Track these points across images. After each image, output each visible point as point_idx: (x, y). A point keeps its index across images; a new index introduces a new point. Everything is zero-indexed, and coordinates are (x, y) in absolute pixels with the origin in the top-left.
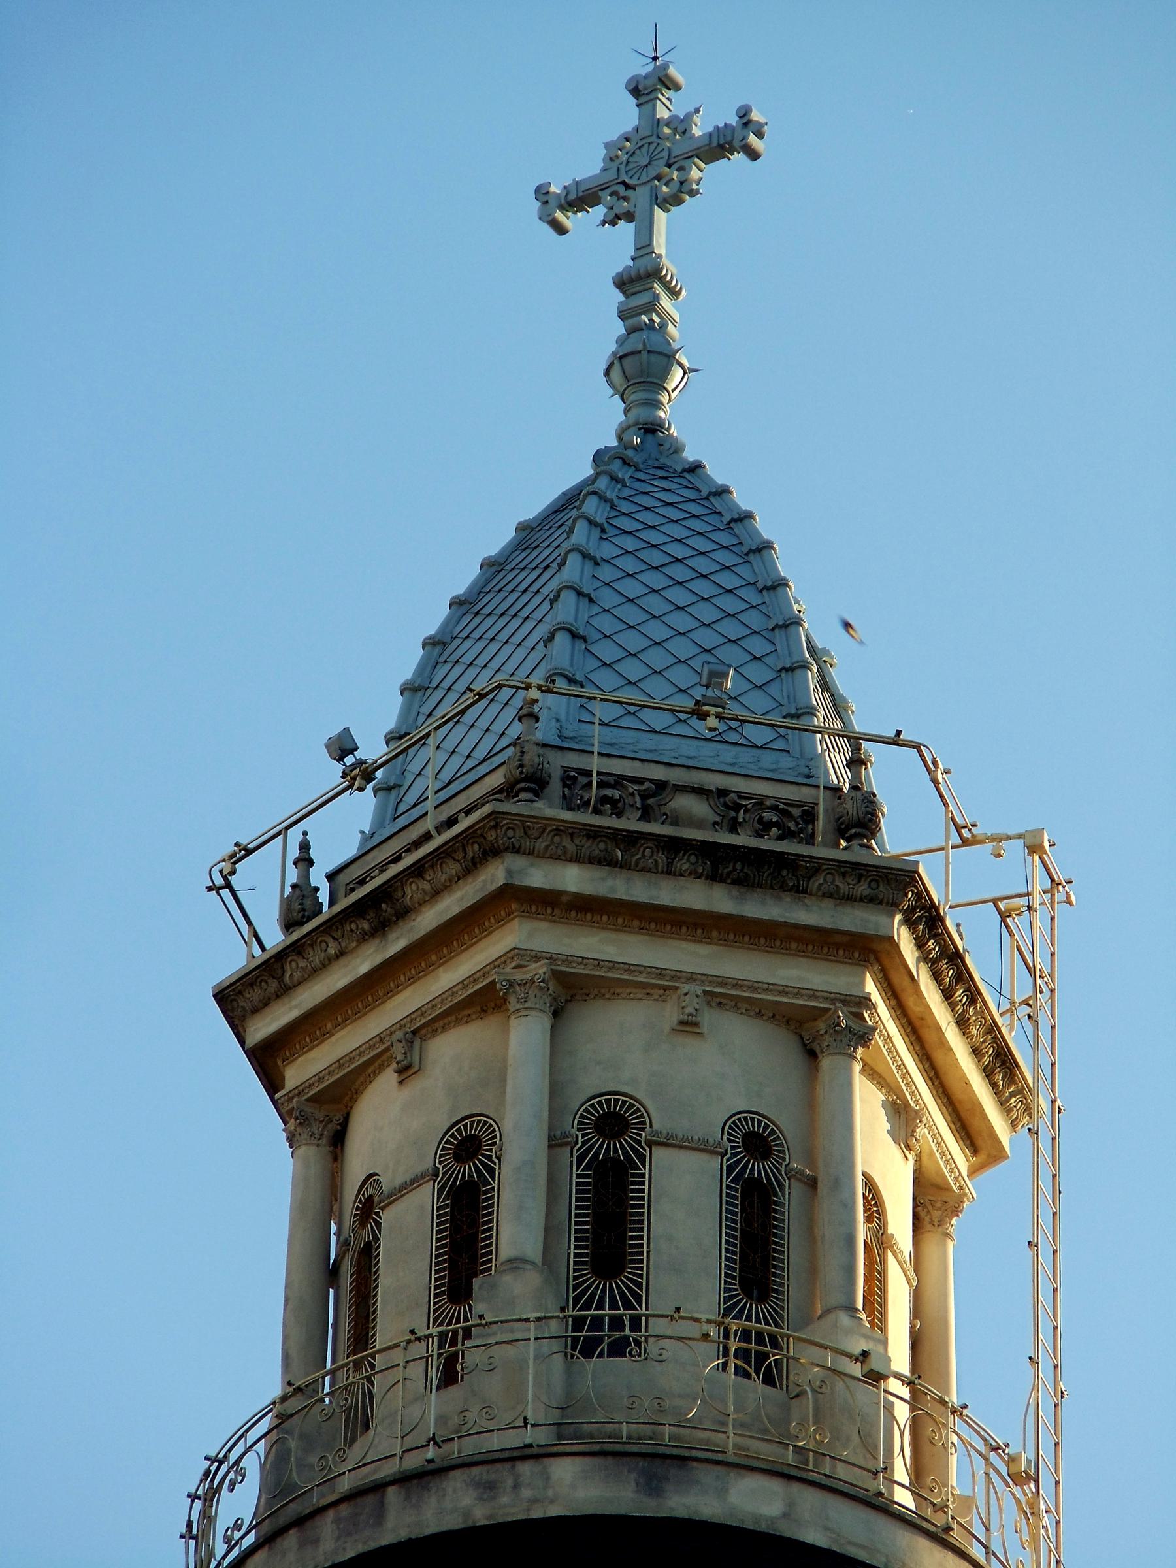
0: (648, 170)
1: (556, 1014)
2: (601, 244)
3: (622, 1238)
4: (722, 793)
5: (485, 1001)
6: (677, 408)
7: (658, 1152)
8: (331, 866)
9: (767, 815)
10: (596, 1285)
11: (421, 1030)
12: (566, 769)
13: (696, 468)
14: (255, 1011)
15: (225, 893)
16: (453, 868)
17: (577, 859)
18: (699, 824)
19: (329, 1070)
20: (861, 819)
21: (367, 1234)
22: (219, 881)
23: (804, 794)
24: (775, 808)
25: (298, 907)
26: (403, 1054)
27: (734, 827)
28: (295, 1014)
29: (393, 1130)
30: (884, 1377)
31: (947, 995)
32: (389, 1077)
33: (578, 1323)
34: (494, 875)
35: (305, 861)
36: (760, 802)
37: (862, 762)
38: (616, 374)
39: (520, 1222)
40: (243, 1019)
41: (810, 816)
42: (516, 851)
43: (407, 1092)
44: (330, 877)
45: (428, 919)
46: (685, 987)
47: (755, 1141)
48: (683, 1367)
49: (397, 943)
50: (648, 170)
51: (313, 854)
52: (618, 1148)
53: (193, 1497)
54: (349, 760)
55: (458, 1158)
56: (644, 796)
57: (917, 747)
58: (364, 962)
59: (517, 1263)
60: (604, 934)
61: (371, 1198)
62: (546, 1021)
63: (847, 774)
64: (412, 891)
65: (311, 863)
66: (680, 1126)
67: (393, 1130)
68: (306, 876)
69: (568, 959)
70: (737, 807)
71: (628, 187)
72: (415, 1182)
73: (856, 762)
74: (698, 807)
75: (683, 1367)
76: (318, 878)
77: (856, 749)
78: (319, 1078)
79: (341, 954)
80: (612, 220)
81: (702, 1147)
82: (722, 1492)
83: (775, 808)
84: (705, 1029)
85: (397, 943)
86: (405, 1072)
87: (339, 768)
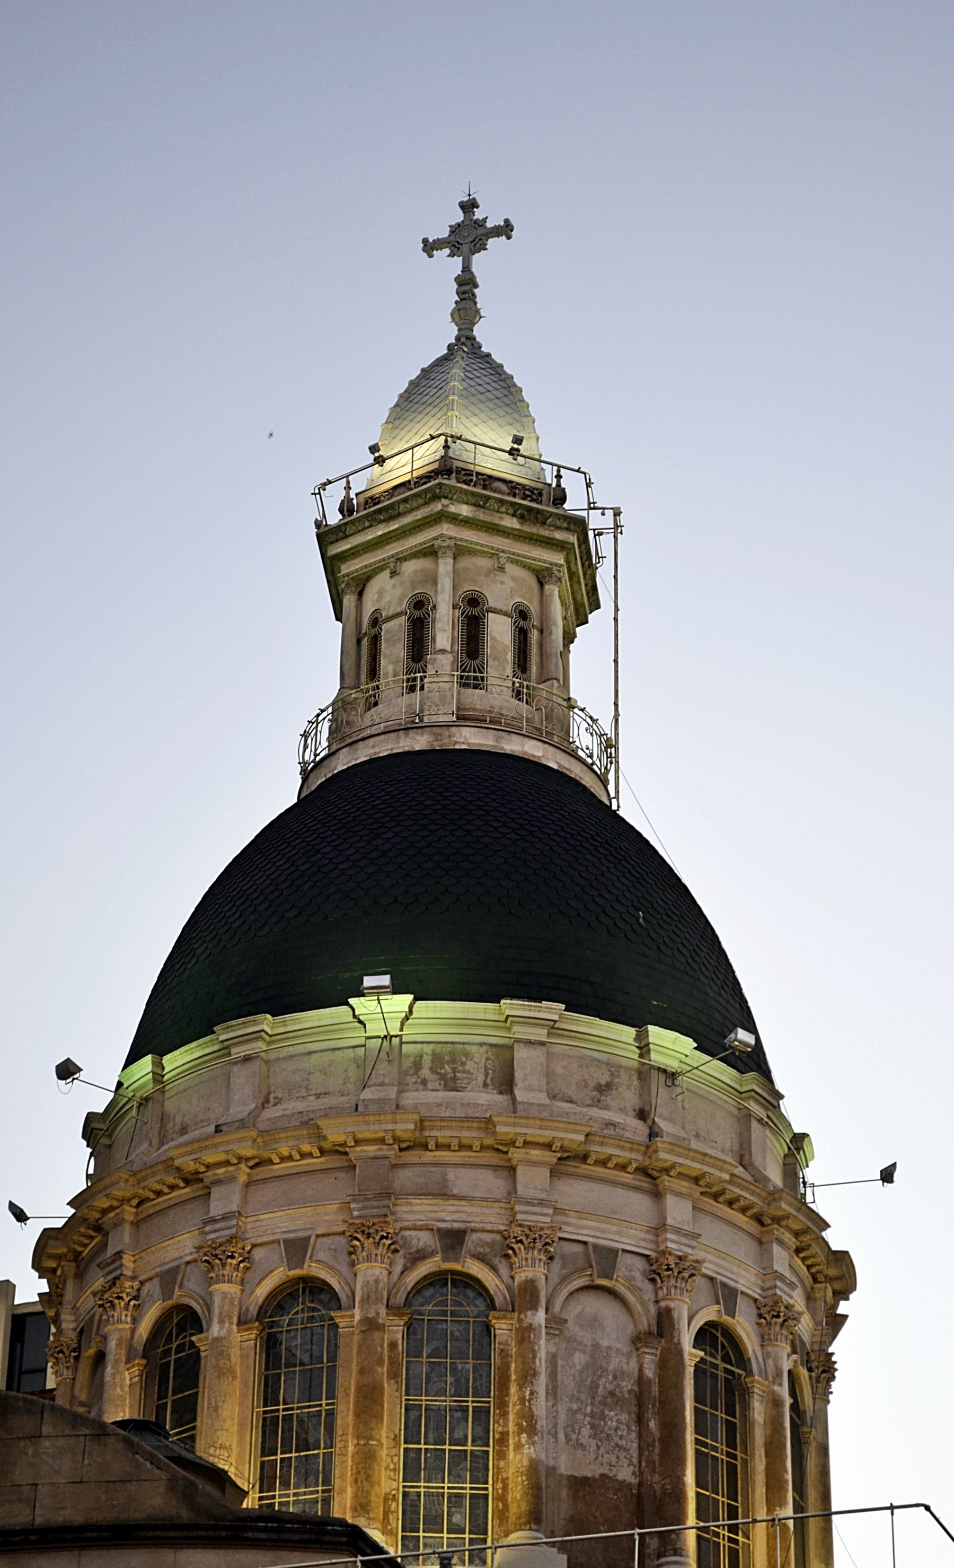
0: (469, 235)
1: (454, 558)
2: (449, 266)
3: (478, 644)
4: (511, 482)
5: (430, 552)
6: (479, 332)
7: (490, 614)
8: (358, 491)
9: (527, 492)
10: (468, 662)
11: (401, 559)
12: (457, 467)
13: (488, 355)
14: (332, 543)
15: (318, 496)
16: (421, 501)
17: (467, 503)
18: (503, 493)
19: (361, 569)
20: (560, 497)
21: (375, 631)
22: (317, 491)
23: (540, 486)
24: (529, 490)
25: (346, 508)
26: (393, 566)
27: (514, 496)
28: (349, 546)
29: (387, 595)
30: (574, 708)
31: (583, 565)
32: (387, 573)
33: (462, 677)
34: (437, 506)
35: (348, 488)
36: (524, 486)
37: (561, 477)
38: (456, 316)
39: (444, 634)
40: (327, 546)
41: (540, 494)
42: (446, 498)
43: (393, 581)
44: (357, 495)
45: (544, 532)
46: (501, 554)
47: (523, 614)
48: (497, 693)
49: (394, 526)
50: (469, 235)
51: (351, 485)
52: (476, 611)
53: (309, 722)
54: (377, 454)
55: (415, 608)
56: (484, 480)
57: (585, 474)
58: (380, 531)
59: (443, 651)
60: (473, 532)
61: (377, 618)
62: (452, 561)
63: (555, 480)
64: (402, 508)
65: (350, 488)
66: (499, 606)
67: (387, 595)
68: (348, 494)
69: (461, 540)
70: (516, 488)
71: (459, 243)
72: (398, 615)
73: (559, 477)
74: (504, 487)
75: (497, 693)
76: (352, 495)
77: (559, 471)
78: (357, 571)
79: (371, 526)
80: (452, 255)
81: (506, 614)
82: (523, 745)
83: (529, 490)
84: (506, 570)
85: (394, 526)
86: (393, 574)
87: (372, 457)
